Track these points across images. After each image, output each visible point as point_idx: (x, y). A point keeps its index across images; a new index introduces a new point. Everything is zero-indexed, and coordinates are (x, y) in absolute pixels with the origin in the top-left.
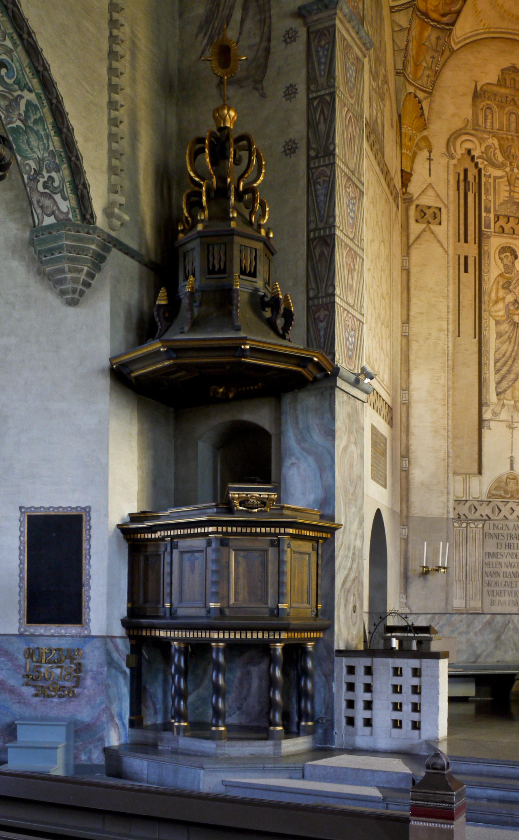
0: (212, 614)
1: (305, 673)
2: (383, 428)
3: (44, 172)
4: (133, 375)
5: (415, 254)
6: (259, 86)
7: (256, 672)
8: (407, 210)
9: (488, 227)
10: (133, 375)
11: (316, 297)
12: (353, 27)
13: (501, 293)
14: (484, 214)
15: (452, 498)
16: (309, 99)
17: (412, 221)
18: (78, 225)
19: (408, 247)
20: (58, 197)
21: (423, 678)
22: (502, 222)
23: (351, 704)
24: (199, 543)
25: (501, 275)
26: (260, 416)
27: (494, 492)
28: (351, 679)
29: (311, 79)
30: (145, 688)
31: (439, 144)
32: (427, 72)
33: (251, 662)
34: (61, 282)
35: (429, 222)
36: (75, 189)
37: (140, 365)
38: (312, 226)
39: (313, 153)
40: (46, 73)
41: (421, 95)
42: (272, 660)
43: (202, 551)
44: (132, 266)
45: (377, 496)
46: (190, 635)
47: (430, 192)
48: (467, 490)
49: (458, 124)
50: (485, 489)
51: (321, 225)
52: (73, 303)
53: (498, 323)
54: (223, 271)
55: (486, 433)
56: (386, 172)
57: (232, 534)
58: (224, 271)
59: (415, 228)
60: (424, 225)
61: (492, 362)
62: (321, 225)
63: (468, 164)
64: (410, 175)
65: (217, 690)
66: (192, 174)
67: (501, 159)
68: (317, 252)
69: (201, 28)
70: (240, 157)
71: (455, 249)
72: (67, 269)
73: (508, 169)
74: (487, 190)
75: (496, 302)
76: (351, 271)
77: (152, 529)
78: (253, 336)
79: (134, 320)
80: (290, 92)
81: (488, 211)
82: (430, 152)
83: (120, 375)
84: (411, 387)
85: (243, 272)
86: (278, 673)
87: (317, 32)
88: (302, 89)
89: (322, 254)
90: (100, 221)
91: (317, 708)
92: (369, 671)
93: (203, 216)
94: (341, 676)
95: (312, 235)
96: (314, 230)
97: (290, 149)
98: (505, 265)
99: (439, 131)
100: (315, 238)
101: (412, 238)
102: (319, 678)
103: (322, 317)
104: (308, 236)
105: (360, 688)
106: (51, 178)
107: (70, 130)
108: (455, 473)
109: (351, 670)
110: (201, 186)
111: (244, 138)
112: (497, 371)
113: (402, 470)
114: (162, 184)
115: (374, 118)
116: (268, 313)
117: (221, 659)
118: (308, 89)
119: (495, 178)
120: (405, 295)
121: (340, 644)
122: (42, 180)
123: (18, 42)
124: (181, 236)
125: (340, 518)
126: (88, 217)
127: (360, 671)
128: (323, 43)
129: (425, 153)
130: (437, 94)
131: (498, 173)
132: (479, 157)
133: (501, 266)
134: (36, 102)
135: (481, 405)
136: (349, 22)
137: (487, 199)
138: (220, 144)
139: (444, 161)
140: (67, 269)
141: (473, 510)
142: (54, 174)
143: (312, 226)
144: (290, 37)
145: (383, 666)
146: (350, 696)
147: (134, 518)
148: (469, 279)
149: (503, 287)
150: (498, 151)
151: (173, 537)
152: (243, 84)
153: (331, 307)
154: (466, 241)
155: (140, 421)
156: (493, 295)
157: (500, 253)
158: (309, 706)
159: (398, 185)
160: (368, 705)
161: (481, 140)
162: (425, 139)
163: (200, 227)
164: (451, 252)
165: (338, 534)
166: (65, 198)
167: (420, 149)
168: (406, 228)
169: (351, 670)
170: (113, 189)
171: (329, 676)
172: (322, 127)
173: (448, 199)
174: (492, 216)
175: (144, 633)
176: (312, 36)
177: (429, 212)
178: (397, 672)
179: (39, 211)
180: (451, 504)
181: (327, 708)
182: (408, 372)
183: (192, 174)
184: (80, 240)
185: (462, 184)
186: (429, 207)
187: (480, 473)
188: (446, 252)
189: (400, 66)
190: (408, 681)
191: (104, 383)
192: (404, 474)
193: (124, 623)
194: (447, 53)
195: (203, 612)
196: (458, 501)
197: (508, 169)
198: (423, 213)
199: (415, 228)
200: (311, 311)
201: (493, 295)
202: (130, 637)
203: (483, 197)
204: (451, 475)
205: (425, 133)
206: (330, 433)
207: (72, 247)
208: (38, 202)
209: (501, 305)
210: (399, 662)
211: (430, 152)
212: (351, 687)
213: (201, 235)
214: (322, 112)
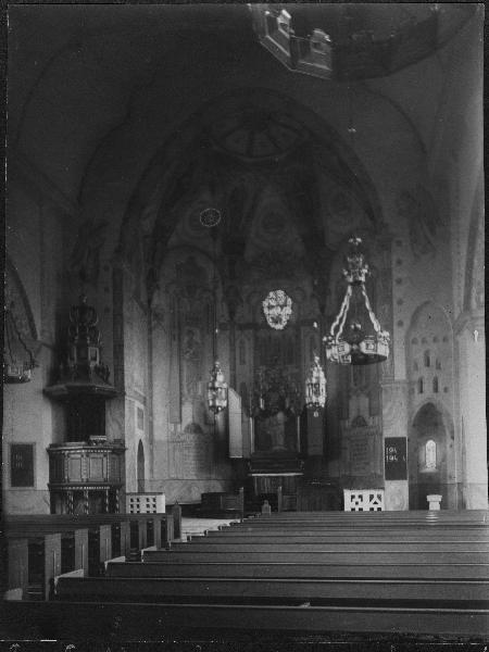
2: (142, 407)
5: (154, 332)
44: (49, 352)
45: (140, 434)
78: (98, 385)
88: (111, 289)
93: (77, 338)
94: (128, 502)
109: (132, 500)
110: (150, 543)
125: (127, 446)
127: (151, 500)
135: (181, 393)
138: (83, 309)
145: (143, 498)
147: (51, 446)
148: (175, 343)
153: (123, 370)
155: (54, 409)
168: (150, 323)
169: (132, 500)
178: (148, 500)
191: (41, 397)
200: (116, 371)
206: (123, 415)
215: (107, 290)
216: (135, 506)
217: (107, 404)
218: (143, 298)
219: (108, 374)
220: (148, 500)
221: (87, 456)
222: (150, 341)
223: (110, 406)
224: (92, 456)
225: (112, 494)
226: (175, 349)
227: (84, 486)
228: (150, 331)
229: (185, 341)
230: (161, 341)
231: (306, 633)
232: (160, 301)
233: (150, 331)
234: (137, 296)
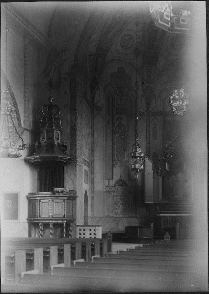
1: (70, 230)
24: (47, 201)
46: (53, 221)
50: (114, 183)
54: (51, 138)
55: (113, 168)
58: (52, 138)
86: (64, 230)
92: (84, 230)
111: (56, 106)
112: (117, 151)
116: (62, 148)
117: (52, 227)
121: (100, 228)
145: (87, 228)
151: (40, 199)
155: (30, 167)
165: (77, 198)
169: (80, 230)
170: (25, 117)
171: (75, 232)
173: (127, 30)
182: (94, 152)
187: (112, 179)
190: (92, 232)
193: (27, 219)
196: (107, 186)
210: (91, 228)
212: (80, 234)
221: (53, 201)
225: (68, 225)
229: (116, 124)
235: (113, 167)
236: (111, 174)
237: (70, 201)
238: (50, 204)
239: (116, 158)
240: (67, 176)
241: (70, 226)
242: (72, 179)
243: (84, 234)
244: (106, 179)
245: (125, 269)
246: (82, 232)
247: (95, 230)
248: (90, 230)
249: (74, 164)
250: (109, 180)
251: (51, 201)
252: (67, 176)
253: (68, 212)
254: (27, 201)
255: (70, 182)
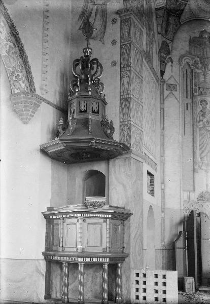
0: (79, 251)
3: (16, 73)
4: (49, 152)
5: (166, 103)
6: (102, 40)
7: (99, 274)
8: (163, 85)
9: (196, 92)
10: (49, 152)
11: (123, 122)
12: (138, 18)
13: (201, 118)
14: (194, 87)
15: (182, 201)
16: (121, 45)
17: (165, 90)
18: (28, 93)
19: (164, 100)
20: (21, 82)
21: (167, 279)
22: (201, 90)
23: (137, 290)
24: (75, 220)
25: (201, 111)
26: (100, 167)
27: (200, 198)
28: (137, 279)
29: (122, 38)
30: (52, 281)
31: (175, 59)
32: (172, 33)
33: (96, 271)
34: (21, 115)
35: (172, 90)
36: (28, 79)
37: (51, 148)
38: (122, 94)
39: (122, 66)
40: (17, 35)
41: (168, 41)
42: (104, 270)
43: (75, 224)
47: (172, 79)
48: (189, 197)
49: (183, 52)
50: (196, 197)
51: (125, 94)
52: (25, 123)
53: (200, 130)
54: (85, 111)
55: (196, 174)
56: (154, 71)
57: (87, 217)
59: (166, 93)
60: (170, 92)
61: (198, 145)
62: (125, 94)
63: (187, 67)
64: (164, 72)
65: (80, 283)
66: (74, 73)
67: (200, 66)
68: (124, 104)
69: (80, 17)
70: (93, 67)
71: (182, 101)
72: (24, 110)
73: (203, 70)
74: (195, 78)
75: (199, 122)
76: (137, 112)
77: (54, 214)
79: (51, 130)
80: (114, 43)
81: (195, 86)
82: (172, 63)
83: (44, 151)
84: (165, 155)
85: (93, 112)
87: (124, 20)
88: (118, 41)
89: (126, 104)
90: (38, 92)
91: (123, 290)
95: (122, 97)
96: (123, 95)
97: (114, 64)
98: (203, 107)
99: (175, 55)
100: (123, 99)
101: (165, 96)
102: (124, 278)
103: (125, 130)
104: (120, 97)
105: (141, 283)
106: (18, 75)
107: (26, 57)
108: (184, 191)
112: (200, 149)
113: (162, 189)
114: (63, 78)
115: (148, 51)
118: (121, 42)
119: (198, 73)
120: (162, 118)
122: (15, 76)
123: (6, 24)
124: (69, 97)
126: (33, 90)
127: (160, 277)
128: (126, 24)
129: (170, 64)
130: (175, 41)
131: (199, 71)
132: (192, 65)
133: (201, 107)
134: (12, 46)
135: (194, 163)
136: (137, 16)
137: (195, 81)
139: (178, 66)
140: (24, 110)
141: (201, 206)
142: (19, 73)
143: (122, 94)
144: (114, 21)
146: (137, 286)
148: (188, 112)
149: (202, 116)
150: (199, 63)
152: (79, 67)
154: (187, 97)
156: (198, 119)
157: (201, 102)
158: (120, 290)
159: (159, 75)
160: (145, 290)
161: (193, 59)
162: (170, 58)
163: (76, 94)
164: (181, 102)
166: (23, 83)
167: (168, 62)
168: (162, 93)
171: (128, 278)
172: (126, 56)
174: (197, 88)
175: (51, 258)
176: (122, 22)
177: (172, 86)
179: (13, 87)
180: (182, 203)
181: (128, 292)
182: (164, 149)
183: (74, 73)
184: (30, 99)
185: (185, 75)
186: (172, 84)
187: (194, 190)
188: (179, 102)
189: (159, 31)
190: (160, 280)
191: (39, 155)
192: (163, 191)
193: (43, 254)
194: (179, 25)
195: (75, 250)
196: (185, 202)
197: (203, 70)
198: (169, 86)
199: (166, 93)
201: (198, 119)
202: (45, 259)
203: (194, 80)
204: (182, 192)
205: (170, 56)
207: (26, 101)
208: (13, 84)
209: (201, 123)
211: (172, 63)
212: (137, 282)
213: (77, 97)
214: (126, 50)
215: (114, 43)
216: (141, 291)
217: (58, 103)
218: (157, 68)
219: (112, 129)
220: (156, 276)
221: (84, 221)
222: (163, 110)
223: (114, 166)
224: (88, 221)
225: (113, 268)
226: (188, 119)
227: (78, 257)
228: (163, 101)
229: (199, 110)
230: (174, 106)
231: (129, 82)
232: (173, 72)
233: (163, 101)
234: (148, 56)
235: (194, 171)
236: (192, 184)
237: (119, 222)
238: (79, 226)
239: (199, 160)
240: (114, 178)
241: (118, 267)
242: (123, 184)
243: (165, 292)
244: (184, 191)
245: (180, 73)
246: (141, 279)
247: (164, 277)
248: (156, 276)
249: (126, 156)
250: (189, 191)
251: (81, 221)
252: (114, 178)
253: (113, 240)
254: (45, 220)
255: (120, 188)
